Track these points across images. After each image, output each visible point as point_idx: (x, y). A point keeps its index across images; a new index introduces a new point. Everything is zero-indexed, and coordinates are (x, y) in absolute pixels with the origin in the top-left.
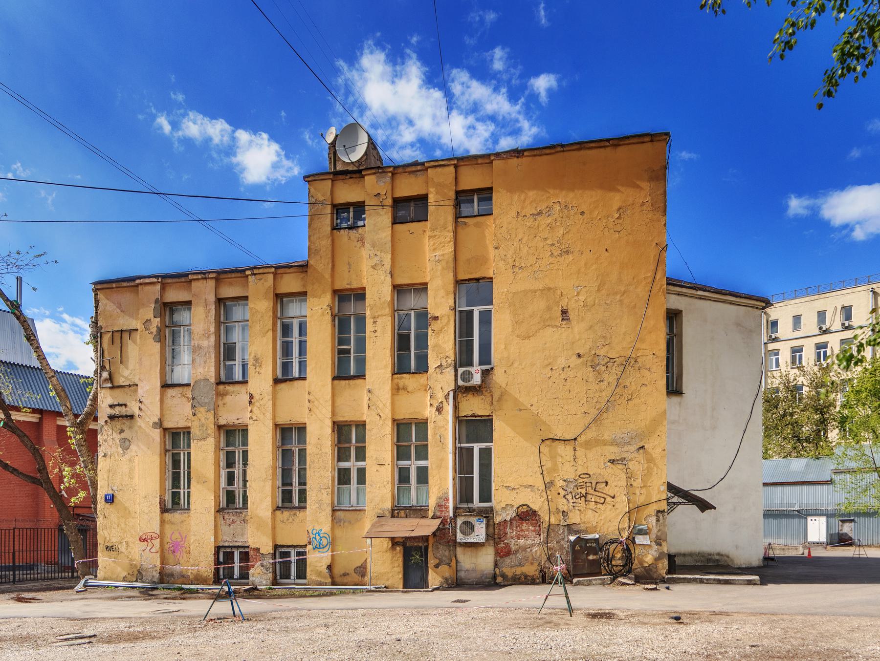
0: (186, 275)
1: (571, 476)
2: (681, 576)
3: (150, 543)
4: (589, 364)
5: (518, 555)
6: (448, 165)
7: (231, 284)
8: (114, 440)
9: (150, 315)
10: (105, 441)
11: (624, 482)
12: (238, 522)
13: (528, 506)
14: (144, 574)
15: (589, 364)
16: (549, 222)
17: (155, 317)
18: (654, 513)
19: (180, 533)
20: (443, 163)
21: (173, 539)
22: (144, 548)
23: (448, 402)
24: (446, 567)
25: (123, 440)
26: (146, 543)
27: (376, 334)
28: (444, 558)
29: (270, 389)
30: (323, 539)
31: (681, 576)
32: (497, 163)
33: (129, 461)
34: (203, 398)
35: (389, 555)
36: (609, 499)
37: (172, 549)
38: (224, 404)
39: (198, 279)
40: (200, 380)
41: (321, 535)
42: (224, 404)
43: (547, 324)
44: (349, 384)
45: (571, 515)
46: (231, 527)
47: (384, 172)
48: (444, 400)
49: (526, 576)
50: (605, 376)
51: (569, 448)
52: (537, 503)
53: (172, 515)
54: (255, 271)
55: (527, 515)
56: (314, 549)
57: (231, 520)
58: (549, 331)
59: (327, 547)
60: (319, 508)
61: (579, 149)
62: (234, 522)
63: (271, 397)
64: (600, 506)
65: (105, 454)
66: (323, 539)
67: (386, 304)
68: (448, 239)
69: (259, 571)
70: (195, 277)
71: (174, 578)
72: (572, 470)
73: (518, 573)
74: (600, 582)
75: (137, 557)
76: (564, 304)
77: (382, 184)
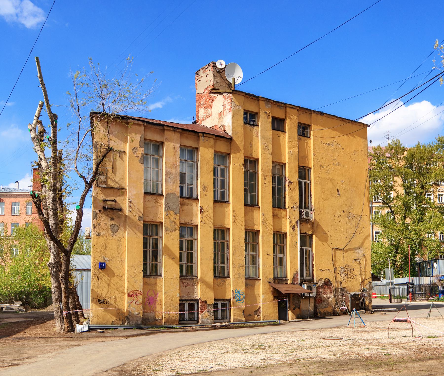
0: (163, 125)
1: (342, 266)
2: (378, 309)
3: (135, 298)
4: (347, 216)
5: (325, 303)
6: (295, 109)
7: (187, 138)
8: (106, 225)
9: (138, 145)
10: (99, 224)
11: (359, 269)
12: (191, 285)
13: (328, 279)
14: (131, 319)
15: (347, 216)
16: (332, 149)
17: (140, 147)
18: (368, 283)
19: (154, 291)
20: (294, 107)
21: (149, 295)
22: (131, 301)
23: (297, 226)
24: (298, 309)
25: (112, 226)
26: (133, 298)
27: (266, 185)
28: (297, 305)
29: (212, 206)
30: (241, 295)
31: (378, 309)
32: (313, 115)
33: (117, 241)
34: (172, 205)
35: (272, 303)
36: (355, 277)
37: (148, 302)
38: (183, 210)
39: (169, 130)
40: (170, 193)
41: (240, 293)
42: (183, 210)
43: (333, 195)
44: (251, 209)
45: (343, 283)
46: (187, 287)
47: (269, 102)
48: (295, 224)
49: (328, 312)
50: (352, 222)
51: (341, 252)
52: (332, 278)
53: (148, 279)
54: (205, 135)
55: (328, 283)
56: (236, 301)
57: (187, 283)
58: (334, 198)
59: (243, 300)
60: (239, 277)
61: (342, 121)
62: (188, 284)
63: (212, 210)
64: (352, 279)
65: (99, 234)
66: (241, 295)
67: (270, 170)
68: (295, 145)
69: (206, 314)
70: (169, 128)
71: (149, 322)
72: (342, 263)
73: (325, 311)
74: (362, 313)
75: (125, 309)
76: (338, 187)
77: (268, 107)
